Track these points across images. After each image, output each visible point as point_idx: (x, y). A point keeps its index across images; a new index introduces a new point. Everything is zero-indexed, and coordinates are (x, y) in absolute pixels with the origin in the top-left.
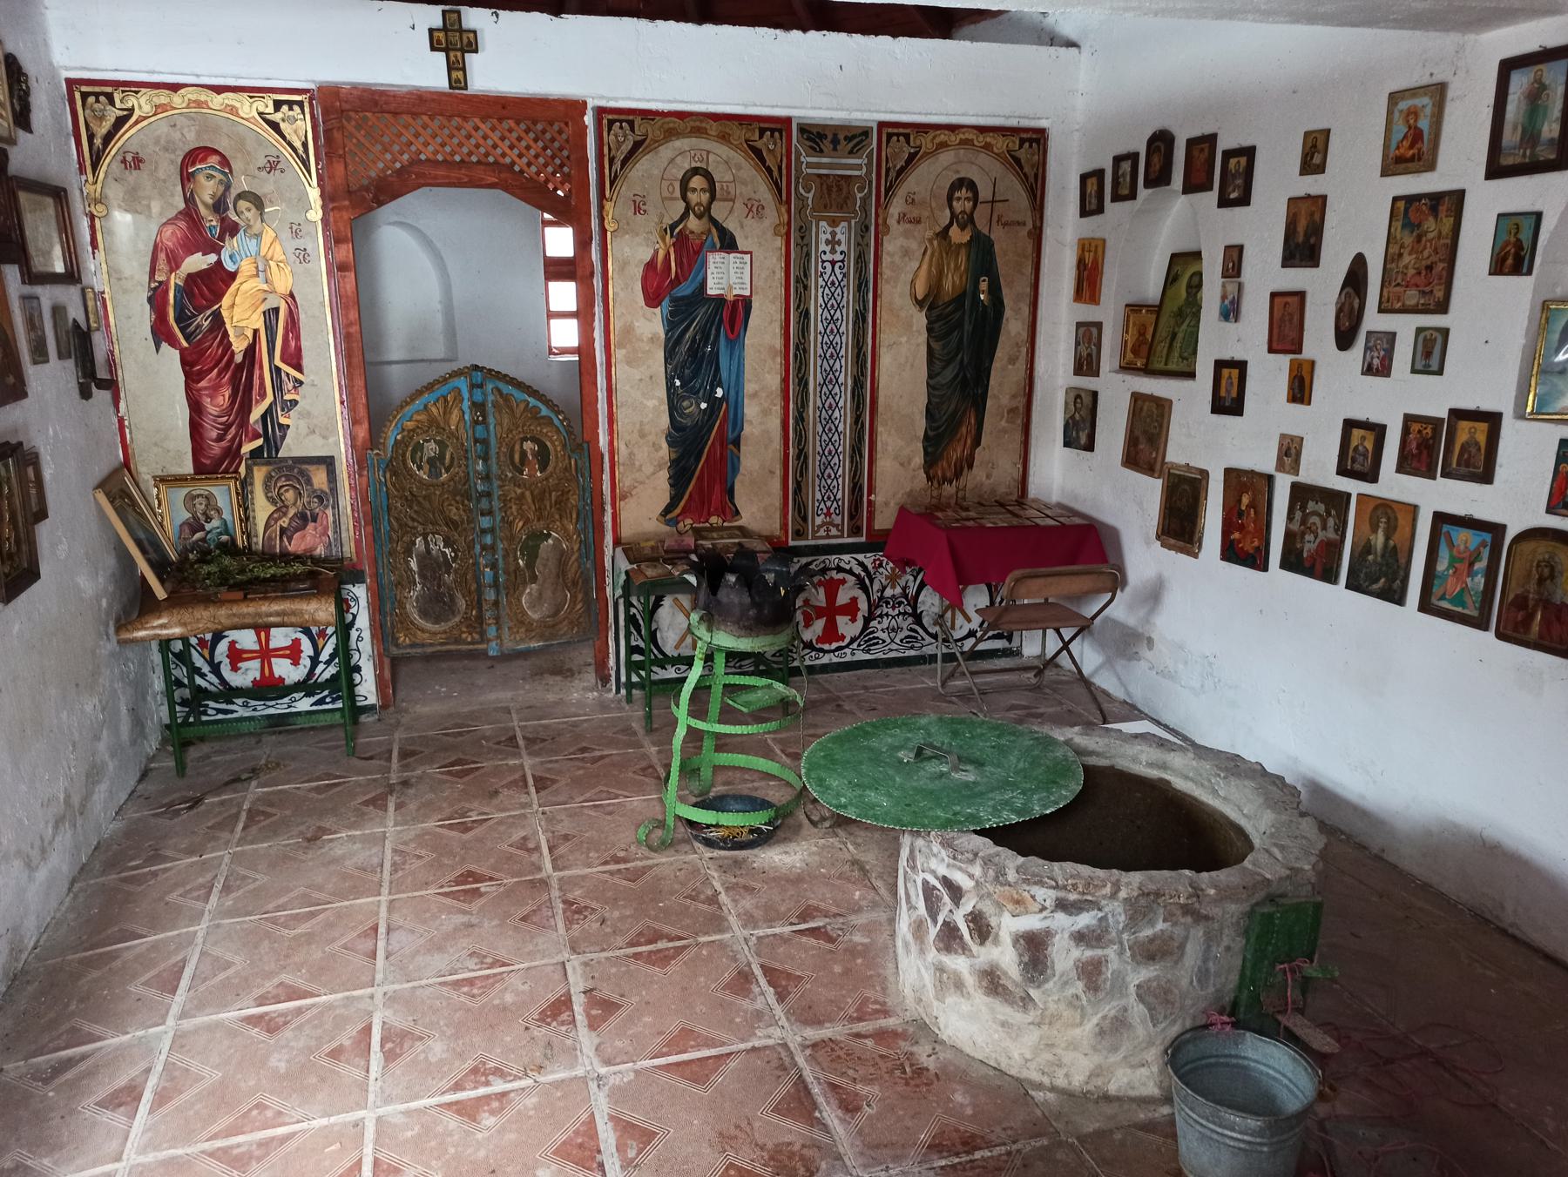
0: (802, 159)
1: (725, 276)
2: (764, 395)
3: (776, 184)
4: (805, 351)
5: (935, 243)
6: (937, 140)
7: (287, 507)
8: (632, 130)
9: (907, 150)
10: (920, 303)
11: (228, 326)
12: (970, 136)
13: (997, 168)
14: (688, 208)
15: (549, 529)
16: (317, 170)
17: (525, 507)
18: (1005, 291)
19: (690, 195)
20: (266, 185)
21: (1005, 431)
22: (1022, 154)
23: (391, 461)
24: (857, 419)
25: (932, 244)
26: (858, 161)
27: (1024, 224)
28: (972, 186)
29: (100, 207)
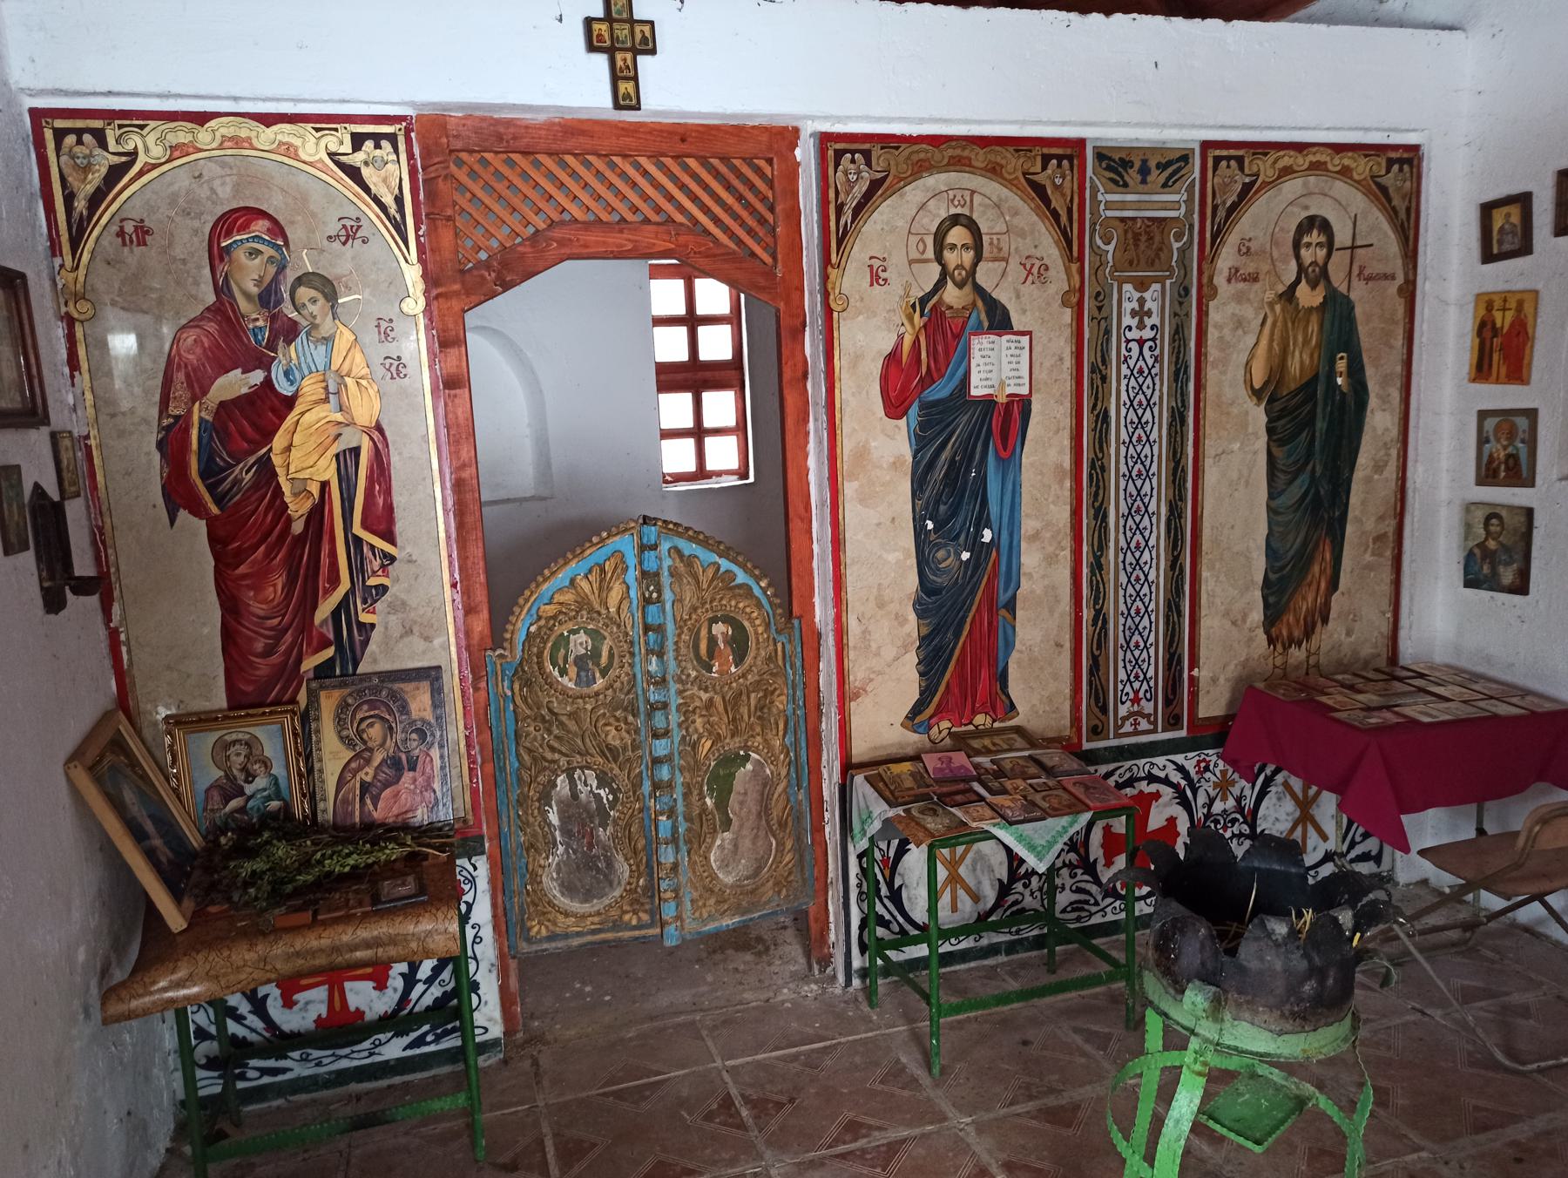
0: (1100, 197)
1: (994, 368)
2: (1048, 535)
3: (1064, 233)
4: (1103, 469)
5: (1278, 308)
6: (1280, 164)
7: (371, 750)
8: (869, 164)
9: (1242, 179)
10: (1257, 394)
11: (282, 480)
12: (1323, 158)
13: (1358, 201)
14: (944, 274)
15: (747, 748)
16: (418, 237)
17: (715, 719)
18: (1370, 372)
19: (947, 254)
20: (340, 262)
21: (1369, 567)
22: (1389, 180)
23: (521, 664)
24: (1174, 563)
25: (1272, 309)
26: (1175, 197)
27: (1393, 277)
28: (1325, 226)
29: (83, 306)
